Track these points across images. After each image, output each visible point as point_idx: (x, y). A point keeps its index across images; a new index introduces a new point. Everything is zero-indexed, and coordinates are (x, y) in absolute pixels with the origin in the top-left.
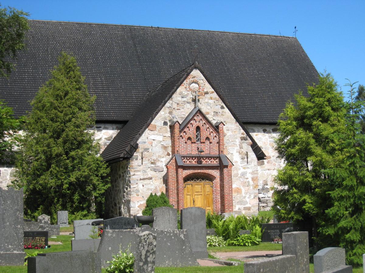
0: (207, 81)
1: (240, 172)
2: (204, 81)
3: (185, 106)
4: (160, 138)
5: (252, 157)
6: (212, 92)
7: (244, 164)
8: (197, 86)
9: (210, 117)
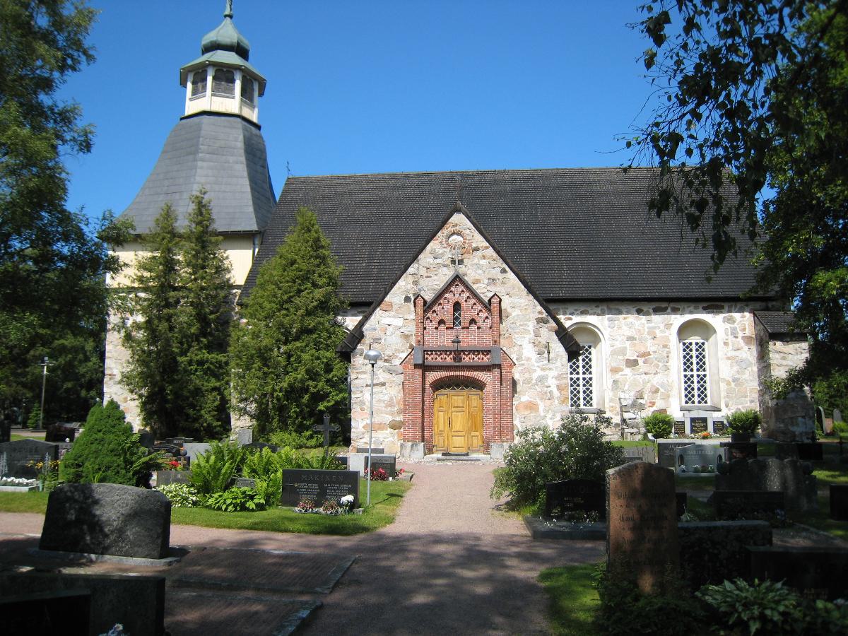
1: (535, 376)
2: (473, 231)
4: (399, 322)
6: (486, 248)
8: (460, 238)
9: (480, 289)
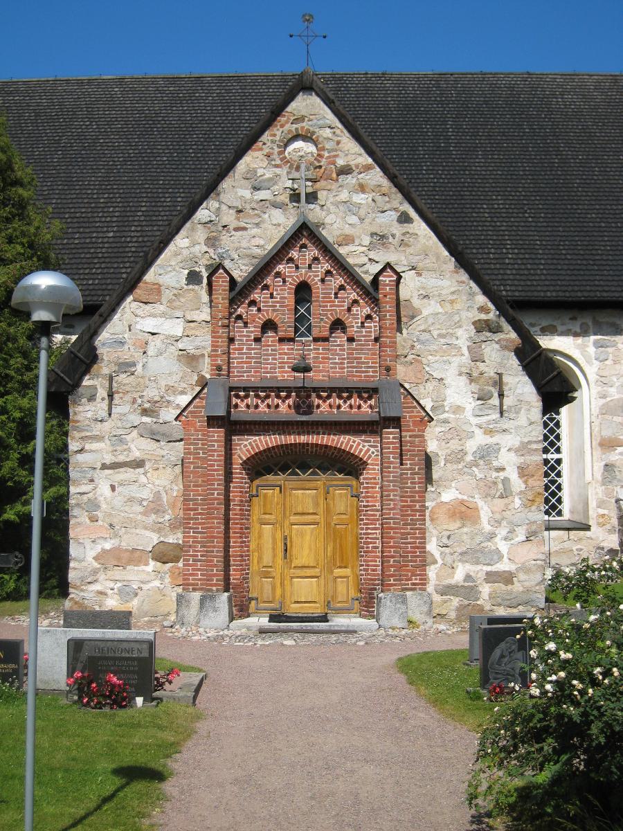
0: (349, 131)
2: (338, 132)
3: (266, 216)
4: (177, 328)
5: (519, 391)
6: (367, 168)
7: (489, 418)
8: (311, 148)
9: (354, 255)
